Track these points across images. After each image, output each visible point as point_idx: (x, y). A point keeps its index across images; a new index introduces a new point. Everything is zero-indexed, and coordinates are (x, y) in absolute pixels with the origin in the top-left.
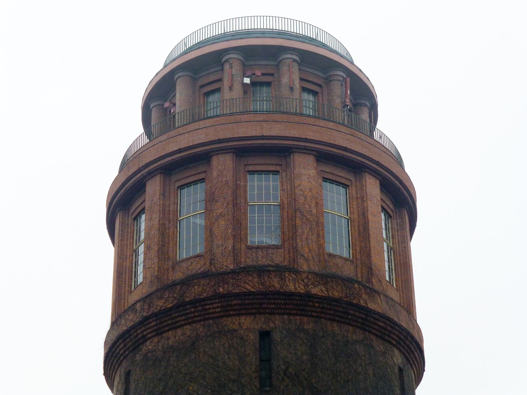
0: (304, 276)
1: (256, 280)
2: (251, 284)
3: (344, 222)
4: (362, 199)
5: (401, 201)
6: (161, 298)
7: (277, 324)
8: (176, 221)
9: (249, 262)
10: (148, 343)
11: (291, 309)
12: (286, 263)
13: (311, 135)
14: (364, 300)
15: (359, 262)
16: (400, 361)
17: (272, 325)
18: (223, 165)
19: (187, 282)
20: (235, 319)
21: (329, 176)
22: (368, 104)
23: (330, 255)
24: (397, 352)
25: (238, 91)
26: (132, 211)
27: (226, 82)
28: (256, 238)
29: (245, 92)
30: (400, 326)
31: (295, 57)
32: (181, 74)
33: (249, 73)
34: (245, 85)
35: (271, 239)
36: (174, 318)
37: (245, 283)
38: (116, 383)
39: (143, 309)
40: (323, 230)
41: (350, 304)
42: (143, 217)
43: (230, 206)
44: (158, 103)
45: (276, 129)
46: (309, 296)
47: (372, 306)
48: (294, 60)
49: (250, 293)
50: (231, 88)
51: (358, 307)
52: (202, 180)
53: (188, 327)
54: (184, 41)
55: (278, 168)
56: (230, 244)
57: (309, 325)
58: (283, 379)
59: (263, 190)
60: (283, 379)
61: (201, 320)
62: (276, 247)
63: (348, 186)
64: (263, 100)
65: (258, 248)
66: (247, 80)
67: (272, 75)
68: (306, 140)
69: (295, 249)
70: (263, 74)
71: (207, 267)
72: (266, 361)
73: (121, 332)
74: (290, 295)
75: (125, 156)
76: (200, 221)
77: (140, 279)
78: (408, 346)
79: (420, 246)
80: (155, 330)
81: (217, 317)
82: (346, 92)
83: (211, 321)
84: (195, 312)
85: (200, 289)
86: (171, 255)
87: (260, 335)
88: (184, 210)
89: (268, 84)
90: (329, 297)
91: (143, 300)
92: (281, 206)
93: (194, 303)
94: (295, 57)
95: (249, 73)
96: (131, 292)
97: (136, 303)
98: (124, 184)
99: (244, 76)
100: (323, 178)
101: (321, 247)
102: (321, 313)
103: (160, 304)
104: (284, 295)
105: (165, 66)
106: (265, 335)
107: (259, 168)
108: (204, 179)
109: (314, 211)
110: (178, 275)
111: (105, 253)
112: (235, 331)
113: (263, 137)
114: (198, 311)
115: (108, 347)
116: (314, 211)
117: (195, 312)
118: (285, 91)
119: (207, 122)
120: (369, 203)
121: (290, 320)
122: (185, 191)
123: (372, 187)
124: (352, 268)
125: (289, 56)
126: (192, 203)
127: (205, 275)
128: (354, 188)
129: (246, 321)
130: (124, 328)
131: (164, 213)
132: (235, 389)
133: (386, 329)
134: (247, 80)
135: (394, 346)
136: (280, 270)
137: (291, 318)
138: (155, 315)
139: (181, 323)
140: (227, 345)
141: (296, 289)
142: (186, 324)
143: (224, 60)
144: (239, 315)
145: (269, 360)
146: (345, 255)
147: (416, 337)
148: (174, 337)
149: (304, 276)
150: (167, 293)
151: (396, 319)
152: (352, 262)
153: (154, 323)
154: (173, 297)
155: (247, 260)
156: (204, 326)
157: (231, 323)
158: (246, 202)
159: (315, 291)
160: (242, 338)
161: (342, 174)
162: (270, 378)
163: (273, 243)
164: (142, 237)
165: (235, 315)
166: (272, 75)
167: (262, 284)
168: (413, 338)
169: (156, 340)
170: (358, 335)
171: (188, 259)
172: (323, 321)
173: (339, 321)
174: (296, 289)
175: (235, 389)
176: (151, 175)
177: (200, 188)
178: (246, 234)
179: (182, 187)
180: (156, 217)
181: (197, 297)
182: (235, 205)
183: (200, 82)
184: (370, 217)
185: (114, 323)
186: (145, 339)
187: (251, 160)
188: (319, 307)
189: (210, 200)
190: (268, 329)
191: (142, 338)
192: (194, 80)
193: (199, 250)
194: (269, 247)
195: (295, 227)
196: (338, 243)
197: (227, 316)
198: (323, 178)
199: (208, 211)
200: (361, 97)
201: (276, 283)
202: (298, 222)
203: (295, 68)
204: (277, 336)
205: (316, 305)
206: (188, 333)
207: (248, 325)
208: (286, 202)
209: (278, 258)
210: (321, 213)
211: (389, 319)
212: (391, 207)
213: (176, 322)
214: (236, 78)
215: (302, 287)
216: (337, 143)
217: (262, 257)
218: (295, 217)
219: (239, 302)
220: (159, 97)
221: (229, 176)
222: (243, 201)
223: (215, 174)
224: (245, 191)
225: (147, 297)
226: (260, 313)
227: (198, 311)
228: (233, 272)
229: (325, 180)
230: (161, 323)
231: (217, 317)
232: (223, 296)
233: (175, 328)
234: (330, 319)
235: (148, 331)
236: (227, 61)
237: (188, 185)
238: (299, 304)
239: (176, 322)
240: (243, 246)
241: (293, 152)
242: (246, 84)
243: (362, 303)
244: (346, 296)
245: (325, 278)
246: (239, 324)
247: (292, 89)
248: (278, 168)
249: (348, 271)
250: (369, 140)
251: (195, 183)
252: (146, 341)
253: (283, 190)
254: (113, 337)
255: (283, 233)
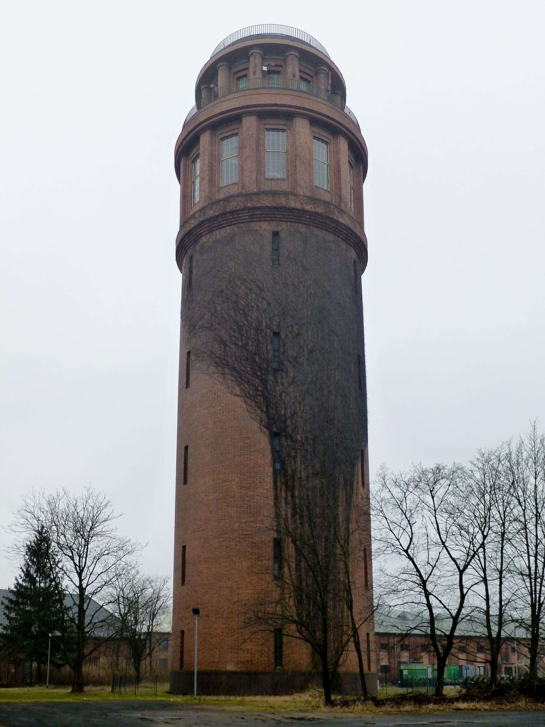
0: (301, 198)
1: (271, 199)
2: (267, 202)
3: (325, 167)
4: (337, 152)
5: (359, 156)
6: (211, 209)
7: (283, 227)
8: (219, 162)
9: (267, 188)
10: (203, 238)
11: (292, 219)
12: (289, 190)
13: (307, 106)
14: (336, 216)
15: (333, 193)
16: (354, 256)
17: (280, 228)
18: (250, 123)
19: (228, 199)
20: (258, 224)
21: (317, 135)
22: (340, 93)
23: (316, 187)
24: (353, 251)
25: (259, 74)
26: (191, 157)
27: (251, 70)
28: (270, 173)
29: (264, 76)
30: (357, 235)
31: (296, 54)
32: (221, 64)
33: (266, 63)
34: (264, 72)
35: (280, 174)
36: (219, 222)
37: (264, 201)
38: (184, 264)
39: (200, 216)
40: (313, 170)
41: (328, 217)
42: (198, 161)
43: (255, 151)
44: (205, 86)
45: (285, 100)
46: (304, 211)
47: (341, 220)
48: (296, 56)
49: (268, 207)
50: (254, 73)
51: (332, 220)
52: (236, 134)
53: (228, 228)
54: (223, 42)
55: (285, 128)
56: (254, 175)
57: (303, 229)
58: (286, 261)
59: (275, 141)
60: (286, 261)
61: (236, 224)
62: (284, 180)
63: (328, 143)
64: (276, 80)
65: (272, 179)
66: (265, 68)
67: (281, 66)
68: (303, 109)
69: (296, 181)
70: (276, 66)
71: (240, 190)
72: (276, 250)
73: (186, 231)
74: (292, 210)
75: (186, 120)
76: (235, 161)
77: (197, 199)
78: (360, 248)
79: (369, 187)
80: (208, 230)
81: (246, 222)
82: (328, 82)
83: (242, 224)
84: (232, 218)
85: (236, 204)
86: (216, 183)
87: (273, 234)
88: (224, 154)
89: (278, 72)
90: (316, 212)
91: (200, 211)
92: (287, 153)
93: (232, 212)
94: (296, 54)
95: (266, 63)
96: (192, 208)
97: (195, 213)
98: (186, 138)
99: (263, 65)
100: (314, 136)
101: (311, 181)
102: (310, 222)
103: (210, 213)
104: (288, 209)
105: (211, 58)
106: (276, 234)
107: (273, 127)
108: (237, 133)
109: (308, 157)
110: (221, 196)
111: (175, 188)
112: (257, 230)
113: (276, 105)
114: (235, 218)
115: (179, 241)
116: (308, 157)
117: (232, 218)
118: (290, 76)
119: (239, 94)
120: (341, 155)
121: (291, 226)
122: (225, 142)
123: (343, 145)
124: (329, 196)
125: (293, 53)
126: (229, 148)
127: (239, 195)
128: (332, 144)
129: (264, 225)
130: (189, 229)
131: (212, 156)
132: (257, 265)
133: (348, 236)
134: (265, 68)
135: (352, 247)
136: (286, 194)
137: (292, 224)
138: (208, 220)
139: (224, 225)
140: (252, 239)
141: (295, 206)
142: (227, 226)
143: (250, 53)
144: (259, 221)
145: (278, 250)
146: (326, 188)
147: (365, 242)
148: (219, 234)
149: (301, 198)
150: (215, 206)
151: (354, 230)
152: (330, 192)
153: (207, 225)
154: (219, 208)
155: (266, 187)
156: (238, 227)
157: (255, 226)
158: (264, 150)
159: (307, 208)
160: (261, 235)
161: (324, 134)
162: (279, 260)
163: (282, 177)
164: (198, 172)
165: (257, 221)
166: (281, 66)
167: (275, 202)
168: (363, 242)
169: (208, 236)
170: (332, 237)
171: (227, 186)
172: (311, 227)
173: (321, 228)
174: (295, 206)
175: (257, 265)
176: (203, 130)
177: (235, 139)
178: (264, 170)
179: (222, 139)
180: (207, 158)
181: (235, 209)
182: (258, 150)
183: (234, 70)
184: (342, 164)
185: (182, 227)
186: (201, 235)
187: (268, 121)
188: (309, 218)
189: (241, 147)
190: (277, 230)
191: (200, 234)
192: (230, 68)
193: (235, 180)
194: (278, 180)
195: (295, 166)
196: (321, 179)
197: (252, 221)
198: (314, 136)
199: (240, 156)
200: (337, 87)
201: (282, 201)
202: (298, 164)
203: (296, 62)
204: (282, 235)
205: (308, 217)
206: (228, 231)
207: (266, 228)
208: (290, 150)
209: (285, 187)
210: (311, 159)
211: (351, 230)
212: (354, 161)
213: (221, 225)
214: (257, 66)
215: (299, 205)
216: (323, 112)
217: (275, 185)
218: (295, 159)
219: (260, 212)
220: (207, 80)
221: (254, 131)
222: (262, 149)
223: (245, 129)
224: (264, 142)
225: (202, 209)
226: (273, 220)
227: (235, 218)
228: (257, 194)
229: (315, 137)
230: (211, 225)
231: (246, 222)
232: (250, 209)
233: (220, 228)
234: (315, 227)
235: (204, 230)
236: (251, 54)
237: (227, 137)
238: (297, 216)
239: (221, 225)
240: (263, 178)
241: (295, 117)
242: (264, 71)
243: (335, 218)
244: (326, 213)
245: (313, 200)
246: (260, 226)
247: (294, 76)
248: (285, 128)
249: (327, 197)
250: (342, 112)
251: (231, 136)
252: (202, 236)
253: (288, 142)
254: (182, 235)
255: (288, 170)
